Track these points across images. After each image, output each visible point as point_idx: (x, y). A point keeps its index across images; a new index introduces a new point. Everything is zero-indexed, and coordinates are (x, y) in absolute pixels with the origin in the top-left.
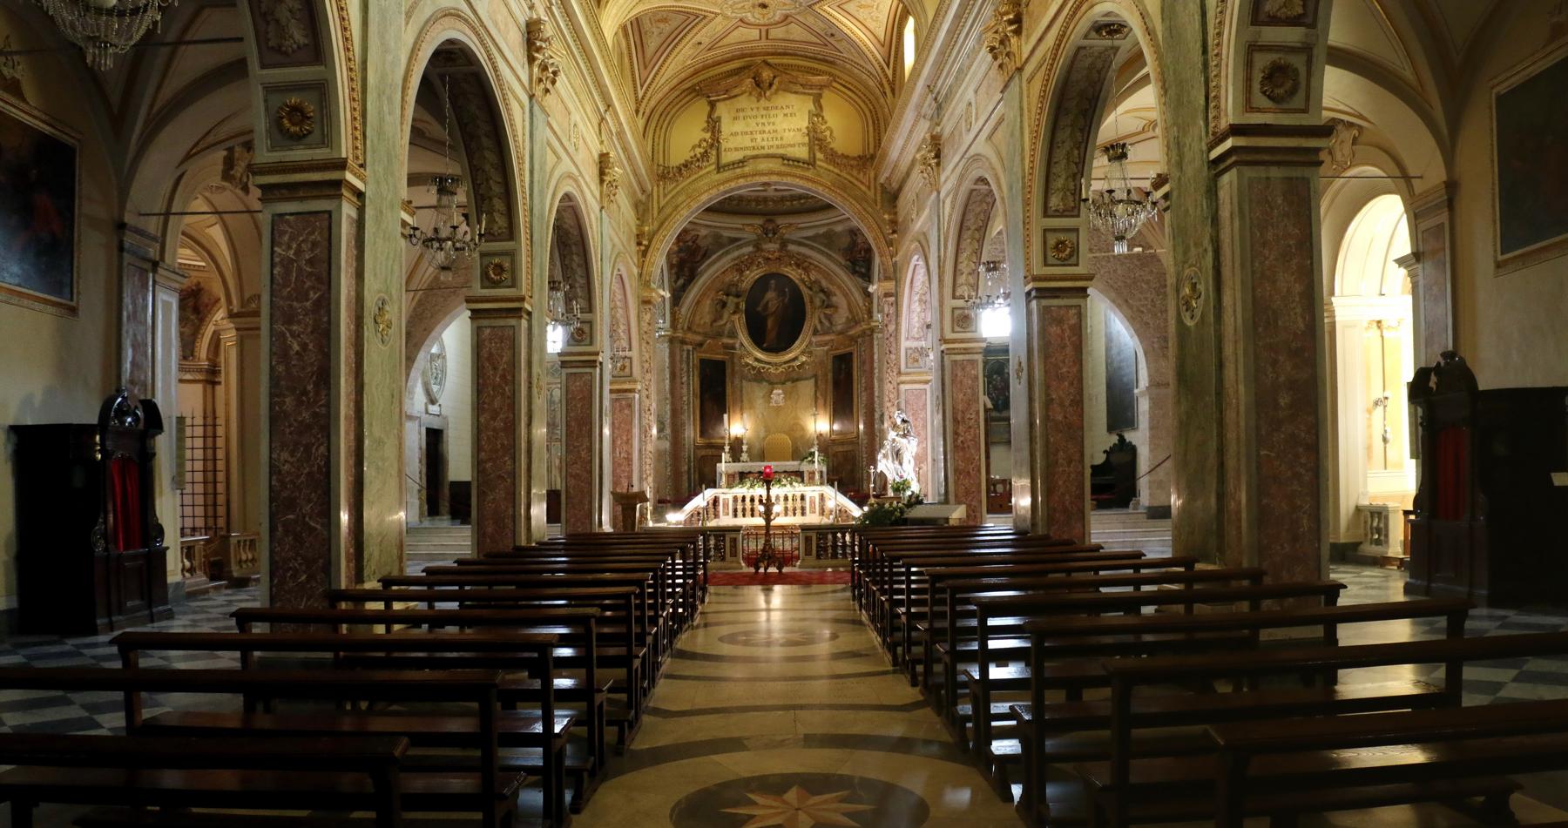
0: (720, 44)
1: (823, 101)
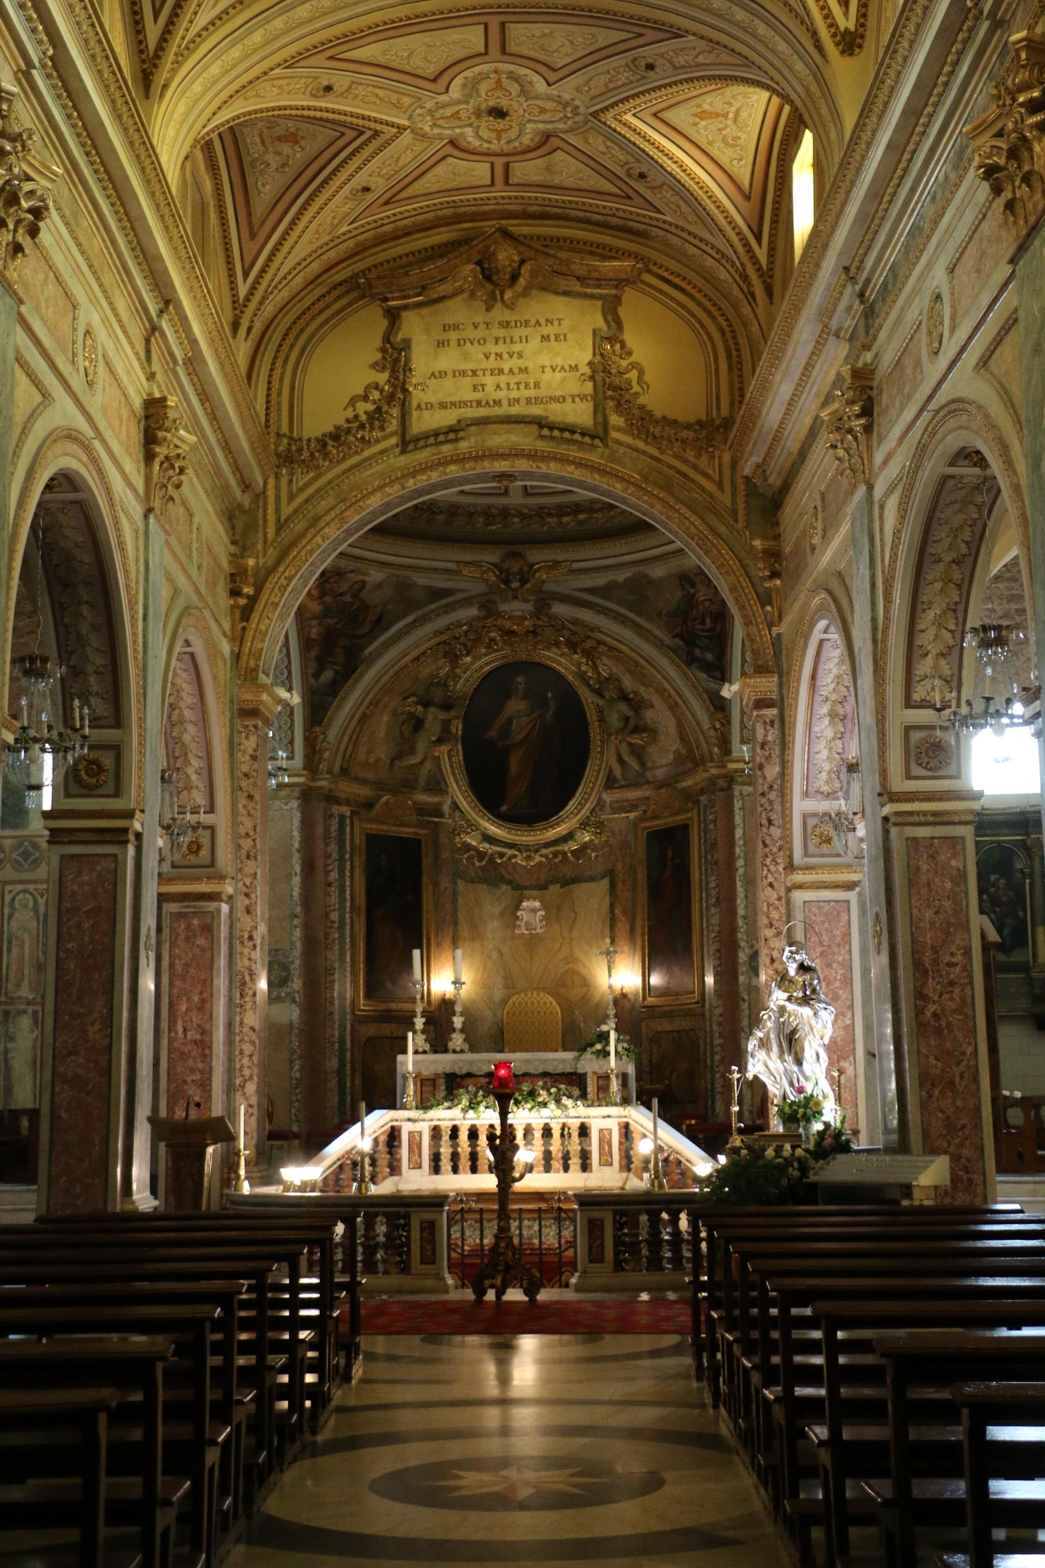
0: (410, 191)
1: (622, 312)
